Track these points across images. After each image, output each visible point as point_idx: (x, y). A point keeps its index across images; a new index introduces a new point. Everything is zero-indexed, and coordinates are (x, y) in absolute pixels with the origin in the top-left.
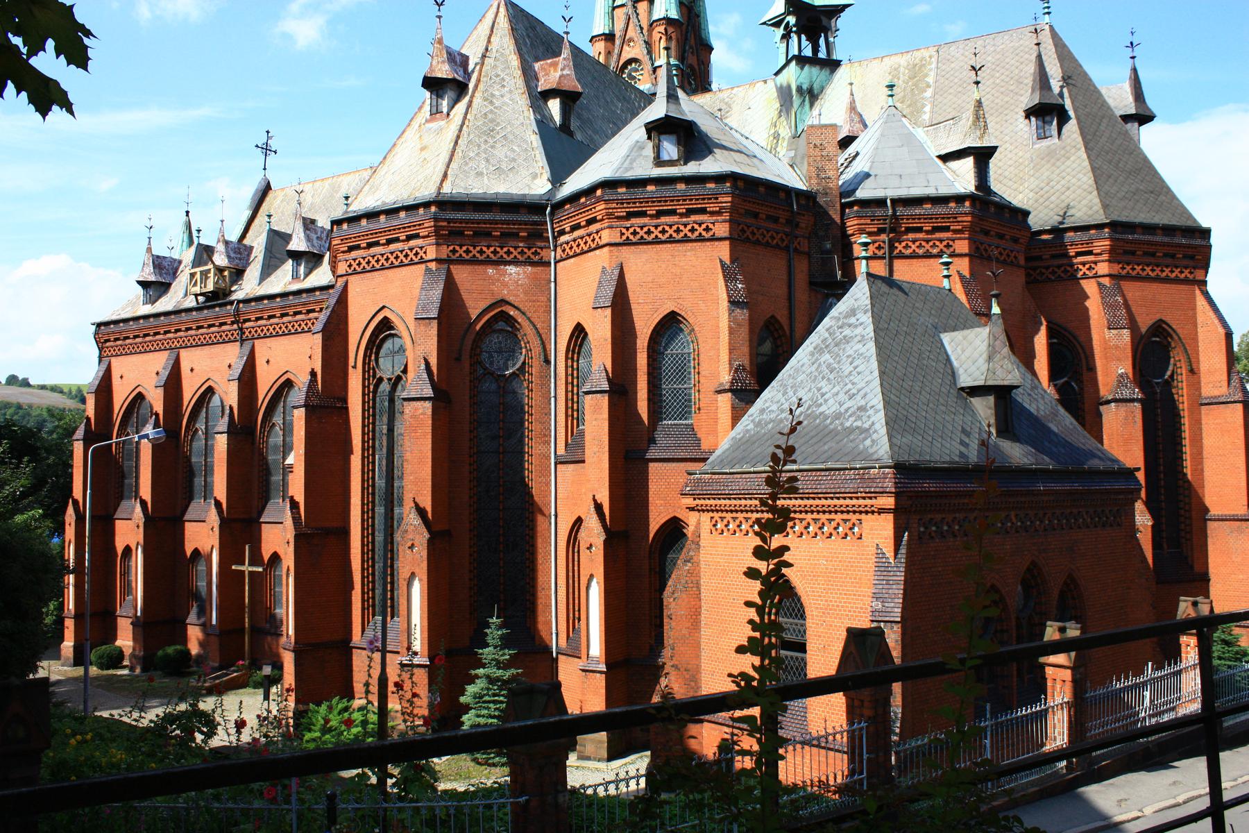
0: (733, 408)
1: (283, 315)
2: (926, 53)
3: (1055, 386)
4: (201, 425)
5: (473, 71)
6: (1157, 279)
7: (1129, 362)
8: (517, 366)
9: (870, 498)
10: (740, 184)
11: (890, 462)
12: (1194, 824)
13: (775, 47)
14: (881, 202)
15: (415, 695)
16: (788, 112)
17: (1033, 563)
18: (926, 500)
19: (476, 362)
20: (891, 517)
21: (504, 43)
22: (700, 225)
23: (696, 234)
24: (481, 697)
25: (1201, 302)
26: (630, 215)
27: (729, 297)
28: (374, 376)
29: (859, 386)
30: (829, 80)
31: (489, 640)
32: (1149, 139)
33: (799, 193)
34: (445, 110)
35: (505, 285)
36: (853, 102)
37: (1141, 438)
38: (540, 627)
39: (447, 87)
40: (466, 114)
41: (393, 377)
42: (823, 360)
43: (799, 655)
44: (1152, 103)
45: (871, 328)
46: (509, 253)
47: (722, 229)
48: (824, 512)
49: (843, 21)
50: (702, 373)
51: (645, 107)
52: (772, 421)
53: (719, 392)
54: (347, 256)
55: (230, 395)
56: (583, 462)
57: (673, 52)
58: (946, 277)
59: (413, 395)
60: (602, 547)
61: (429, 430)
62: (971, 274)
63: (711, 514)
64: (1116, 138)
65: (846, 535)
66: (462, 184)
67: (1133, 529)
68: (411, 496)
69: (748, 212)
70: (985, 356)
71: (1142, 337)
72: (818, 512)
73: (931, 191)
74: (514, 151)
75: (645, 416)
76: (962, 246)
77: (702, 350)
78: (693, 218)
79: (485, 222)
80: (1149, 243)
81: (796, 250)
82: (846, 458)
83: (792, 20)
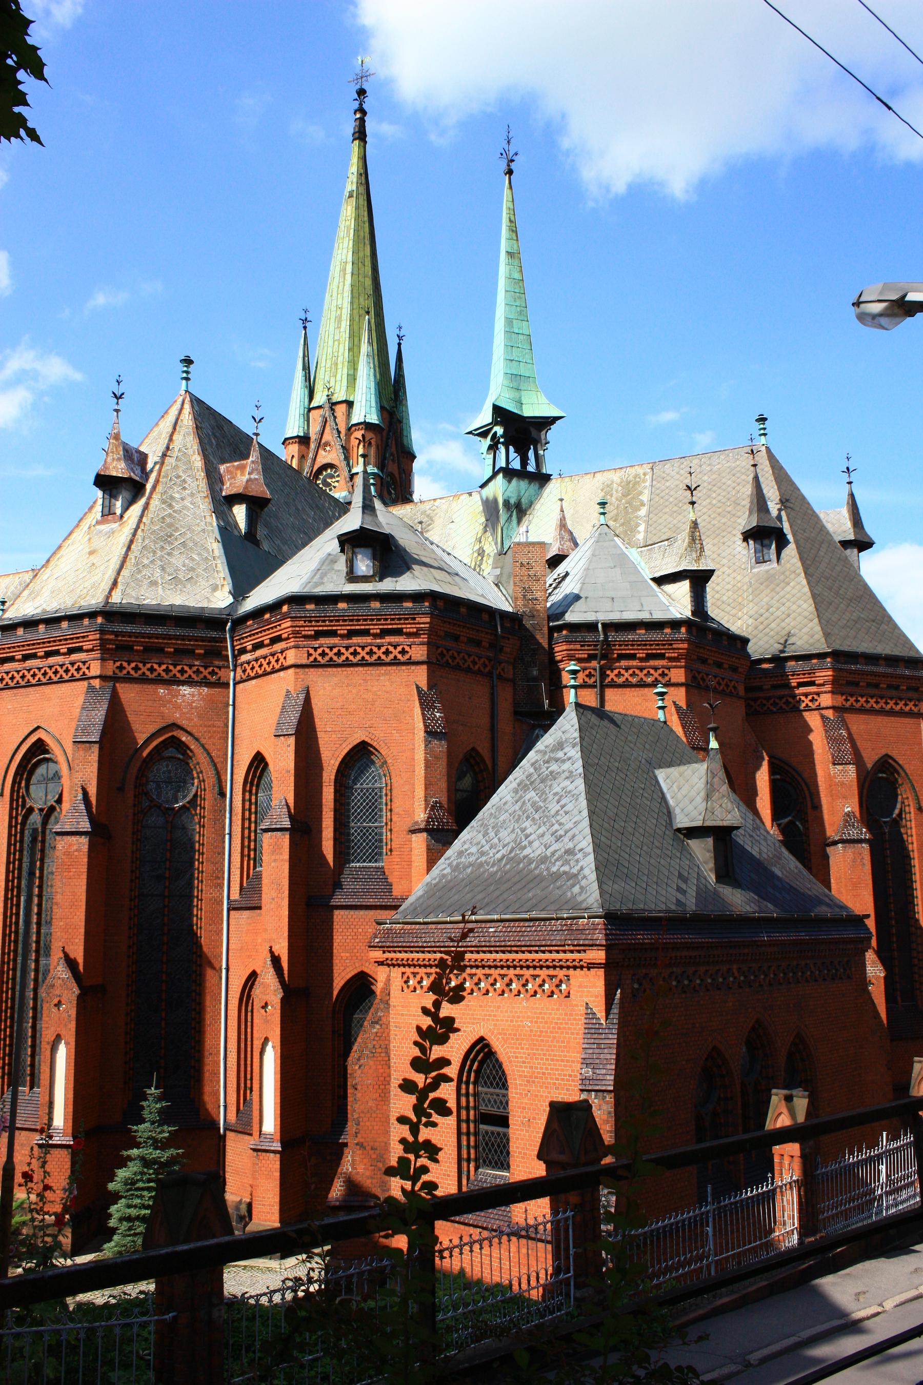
0: (429, 849)
2: (640, 471)
3: (779, 825)
5: (152, 471)
6: (882, 712)
7: (856, 800)
8: (188, 799)
9: (579, 951)
10: (440, 604)
12: (918, 1339)
13: (478, 461)
14: (591, 627)
15: (47, 1188)
20: (601, 972)
21: (187, 442)
22: (395, 647)
23: (391, 656)
24: (133, 1183)
26: (318, 635)
27: (426, 726)
28: (24, 806)
29: (567, 827)
30: (538, 495)
31: (146, 1114)
32: (871, 567)
33: (503, 614)
34: (118, 512)
35: (178, 707)
36: (563, 519)
37: (870, 882)
38: (207, 1098)
39: (122, 486)
40: (142, 516)
42: (527, 797)
43: (501, 1130)
45: (580, 763)
46: (182, 672)
47: (419, 652)
48: (528, 967)
49: (553, 434)
50: (395, 810)
51: (340, 516)
52: (471, 865)
53: (413, 832)
56: (260, 908)
57: (372, 458)
58: (660, 708)
59: (68, 828)
60: (278, 1006)
61: (84, 869)
62: (688, 705)
63: (402, 969)
64: (834, 563)
65: (553, 993)
66: (134, 594)
67: (864, 982)
68: (61, 944)
70: (703, 794)
71: (868, 772)
72: (522, 967)
73: (644, 616)
74: (193, 560)
76: (678, 675)
77: (395, 785)
78: (388, 639)
79: (158, 636)
81: (500, 677)
82: (553, 907)
83: (499, 430)
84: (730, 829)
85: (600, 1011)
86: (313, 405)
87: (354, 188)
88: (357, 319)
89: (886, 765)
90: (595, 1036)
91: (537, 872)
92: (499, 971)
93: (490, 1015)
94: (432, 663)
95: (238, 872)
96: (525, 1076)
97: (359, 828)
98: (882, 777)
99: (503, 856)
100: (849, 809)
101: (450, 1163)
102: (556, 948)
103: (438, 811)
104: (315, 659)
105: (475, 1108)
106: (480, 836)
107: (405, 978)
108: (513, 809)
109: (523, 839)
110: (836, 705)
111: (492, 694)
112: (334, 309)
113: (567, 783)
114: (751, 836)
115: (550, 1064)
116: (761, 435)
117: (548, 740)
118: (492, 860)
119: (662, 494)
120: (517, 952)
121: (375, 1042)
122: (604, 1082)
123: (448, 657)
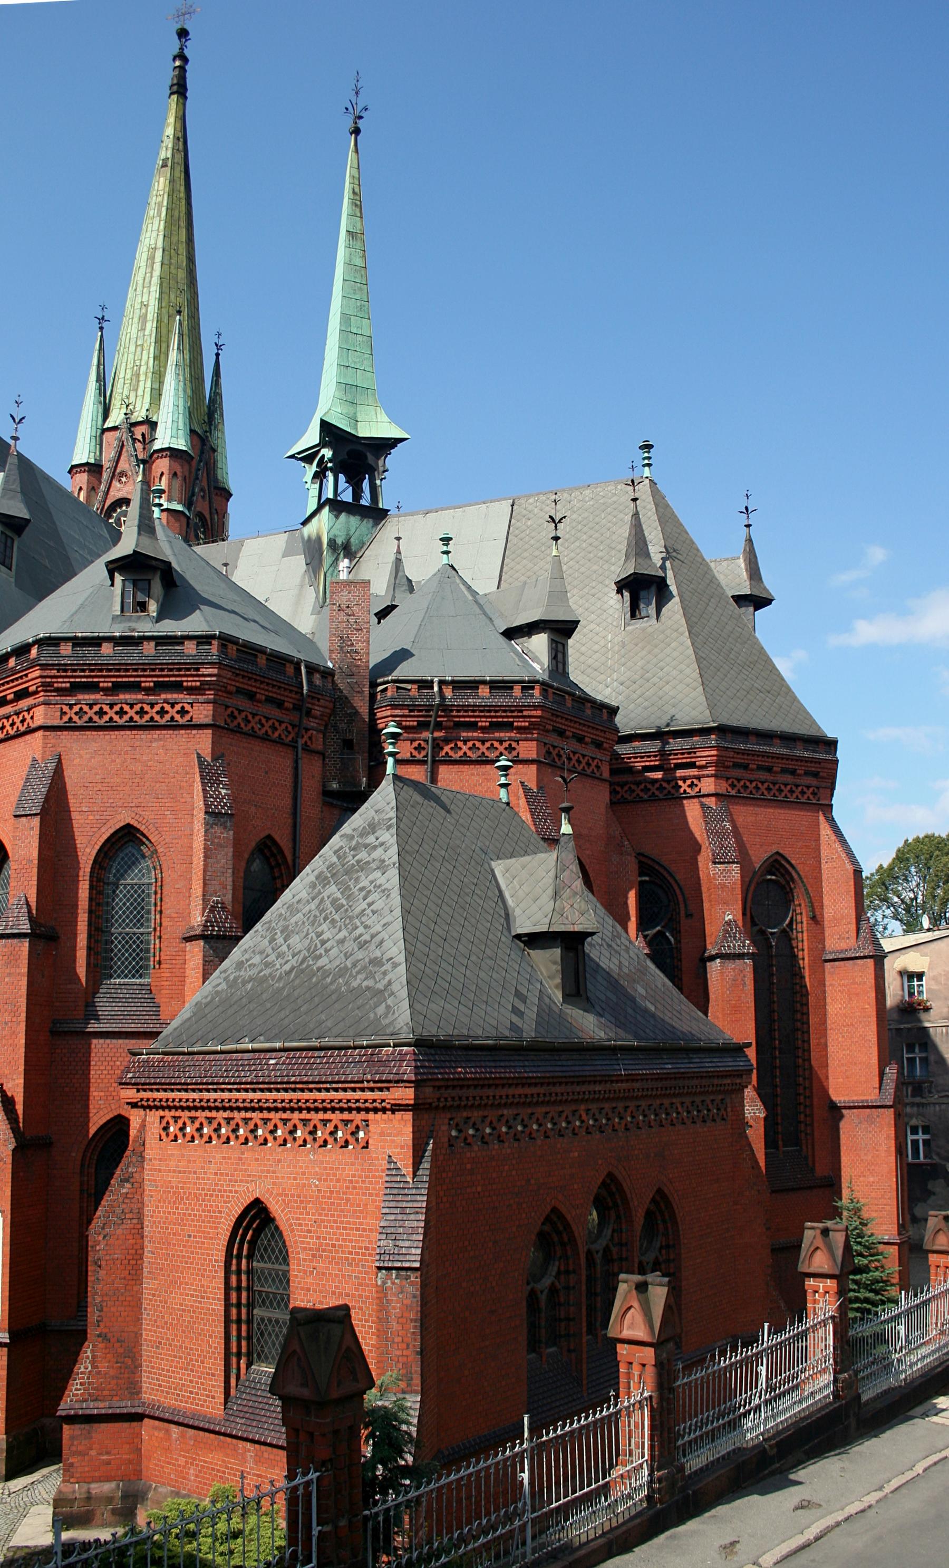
0: (206, 962)
3: (645, 937)
9: (381, 1089)
16: (316, 572)
17: (610, 1175)
18: (458, 1087)
25: (825, 831)
26: (76, 688)
27: (207, 806)
29: (373, 931)
42: (325, 894)
44: (771, 583)
45: (395, 849)
47: (202, 712)
48: (317, 1110)
49: (393, 460)
50: (166, 912)
52: (251, 979)
53: (188, 939)
62: (540, 788)
63: (161, 1113)
67: (742, 1124)
69: (239, 691)
70: (550, 892)
71: (755, 872)
75: (81, 970)
76: (528, 749)
77: (166, 880)
80: (764, 755)
83: (327, 453)
85: (406, 1166)
86: (109, 424)
87: (169, 155)
88: (166, 321)
90: (400, 1198)
91: (333, 987)
92: (281, 1115)
93: (268, 1172)
94: (219, 727)
96: (311, 1249)
97: (120, 934)
98: (770, 880)
99: (293, 968)
100: (730, 917)
101: (216, 1359)
102: (353, 1085)
103: (219, 913)
104: (71, 719)
105: (248, 1289)
106: (266, 942)
107: (164, 1124)
108: (307, 909)
109: (319, 946)
110: (720, 792)
112: (138, 306)
113: (377, 874)
114: (609, 946)
115: (341, 1234)
116: (644, 466)
117: (357, 821)
118: (278, 973)
119: (523, 535)
120: (302, 1090)
121: (124, 1206)
122: (408, 1258)
123: (239, 720)
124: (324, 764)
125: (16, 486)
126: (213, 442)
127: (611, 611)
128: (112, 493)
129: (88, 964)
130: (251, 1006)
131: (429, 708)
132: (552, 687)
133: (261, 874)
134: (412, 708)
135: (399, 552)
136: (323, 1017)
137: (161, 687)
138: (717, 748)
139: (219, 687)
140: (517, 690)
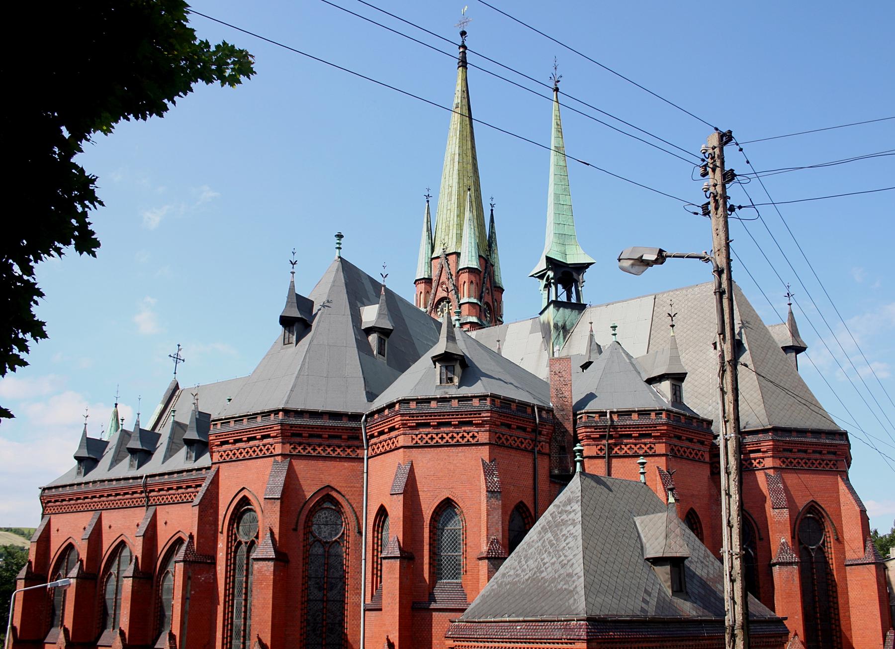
1: (178, 488)
4: (114, 570)
5: (316, 314)
9: (571, 643)
11: (584, 616)
13: (540, 294)
16: (548, 342)
19: (308, 531)
25: (842, 486)
26: (419, 426)
28: (235, 540)
41: (249, 541)
44: (805, 337)
45: (580, 514)
47: (484, 437)
49: (587, 275)
52: (509, 583)
53: (480, 559)
54: (220, 449)
55: (137, 547)
56: (381, 610)
61: (271, 583)
69: (502, 424)
71: (799, 513)
75: (426, 575)
76: (661, 448)
83: (551, 274)
84: (683, 559)
86: (434, 255)
89: (813, 508)
95: (370, 585)
106: (516, 563)
111: (535, 464)
113: (571, 527)
114: (702, 562)
124: (550, 460)
125: (385, 311)
126: (492, 261)
127: (711, 360)
128: (438, 294)
129: (430, 572)
130: (509, 598)
131: (605, 427)
132: (672, 412)
133: (517, 522)
134: (596, 427)
135: (592, 331)
136: (543, 604)
137: (462, 424)
138: (773, 440)
139: (492, 423)
140: (653, 414)
